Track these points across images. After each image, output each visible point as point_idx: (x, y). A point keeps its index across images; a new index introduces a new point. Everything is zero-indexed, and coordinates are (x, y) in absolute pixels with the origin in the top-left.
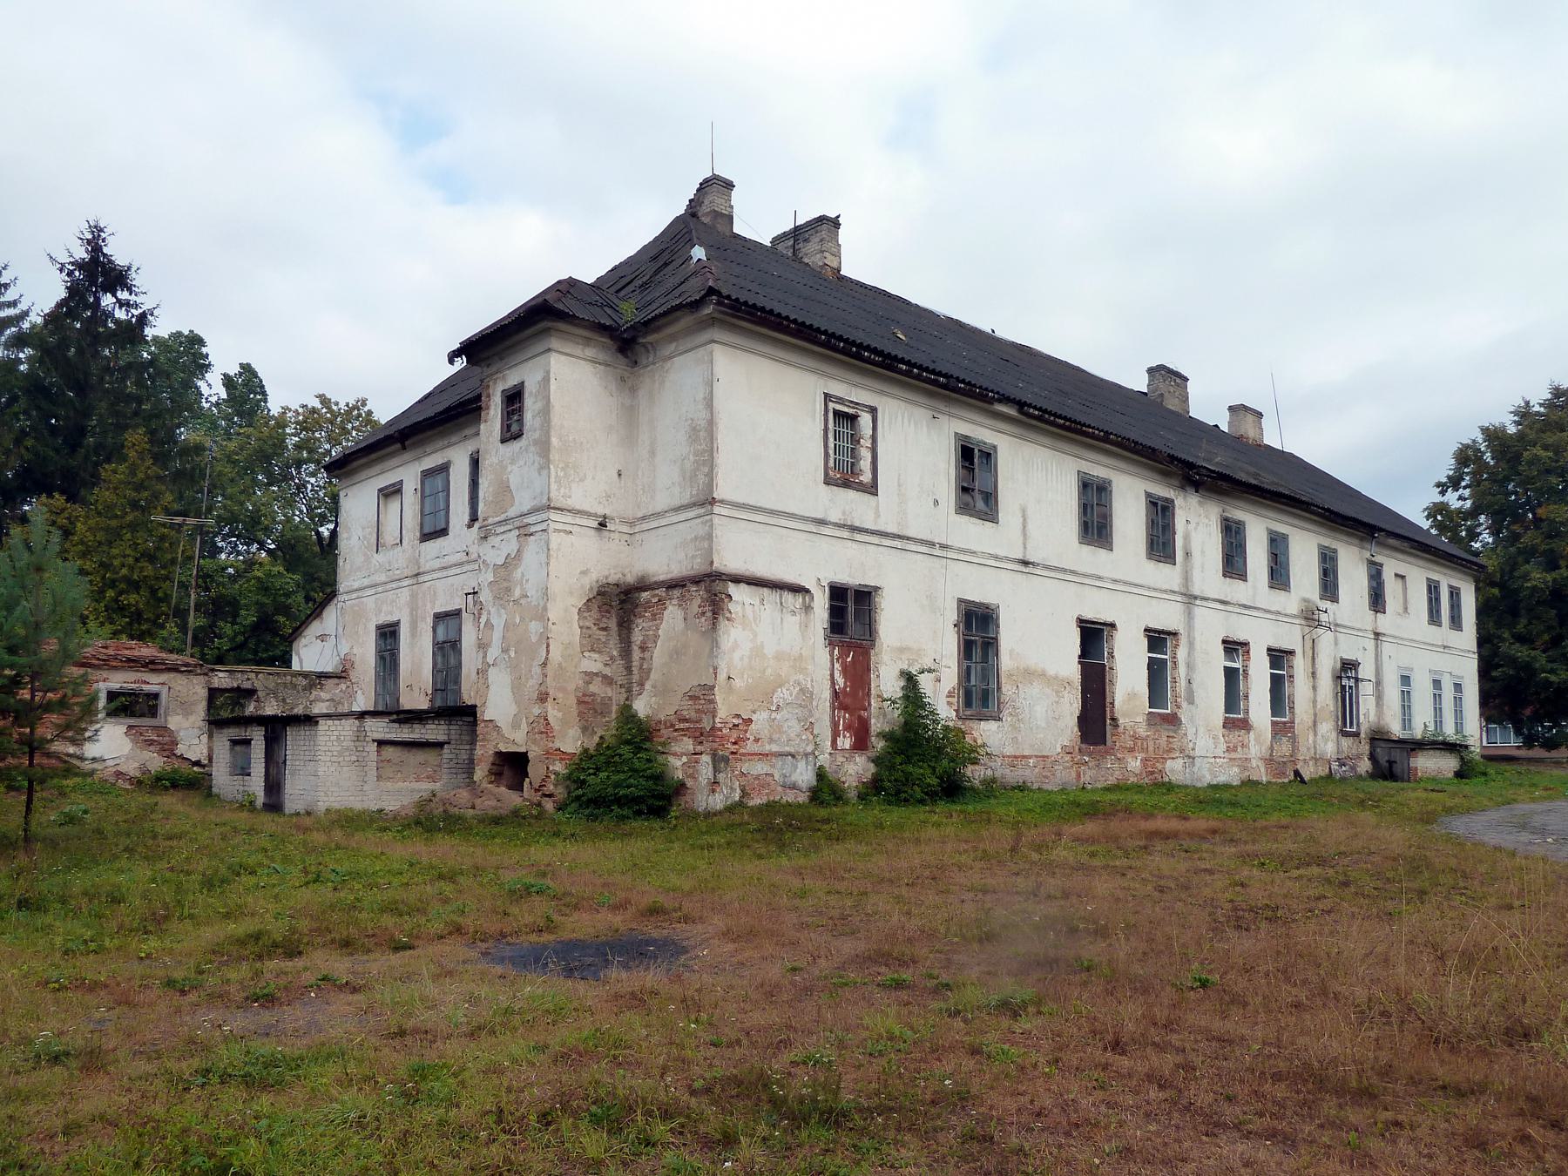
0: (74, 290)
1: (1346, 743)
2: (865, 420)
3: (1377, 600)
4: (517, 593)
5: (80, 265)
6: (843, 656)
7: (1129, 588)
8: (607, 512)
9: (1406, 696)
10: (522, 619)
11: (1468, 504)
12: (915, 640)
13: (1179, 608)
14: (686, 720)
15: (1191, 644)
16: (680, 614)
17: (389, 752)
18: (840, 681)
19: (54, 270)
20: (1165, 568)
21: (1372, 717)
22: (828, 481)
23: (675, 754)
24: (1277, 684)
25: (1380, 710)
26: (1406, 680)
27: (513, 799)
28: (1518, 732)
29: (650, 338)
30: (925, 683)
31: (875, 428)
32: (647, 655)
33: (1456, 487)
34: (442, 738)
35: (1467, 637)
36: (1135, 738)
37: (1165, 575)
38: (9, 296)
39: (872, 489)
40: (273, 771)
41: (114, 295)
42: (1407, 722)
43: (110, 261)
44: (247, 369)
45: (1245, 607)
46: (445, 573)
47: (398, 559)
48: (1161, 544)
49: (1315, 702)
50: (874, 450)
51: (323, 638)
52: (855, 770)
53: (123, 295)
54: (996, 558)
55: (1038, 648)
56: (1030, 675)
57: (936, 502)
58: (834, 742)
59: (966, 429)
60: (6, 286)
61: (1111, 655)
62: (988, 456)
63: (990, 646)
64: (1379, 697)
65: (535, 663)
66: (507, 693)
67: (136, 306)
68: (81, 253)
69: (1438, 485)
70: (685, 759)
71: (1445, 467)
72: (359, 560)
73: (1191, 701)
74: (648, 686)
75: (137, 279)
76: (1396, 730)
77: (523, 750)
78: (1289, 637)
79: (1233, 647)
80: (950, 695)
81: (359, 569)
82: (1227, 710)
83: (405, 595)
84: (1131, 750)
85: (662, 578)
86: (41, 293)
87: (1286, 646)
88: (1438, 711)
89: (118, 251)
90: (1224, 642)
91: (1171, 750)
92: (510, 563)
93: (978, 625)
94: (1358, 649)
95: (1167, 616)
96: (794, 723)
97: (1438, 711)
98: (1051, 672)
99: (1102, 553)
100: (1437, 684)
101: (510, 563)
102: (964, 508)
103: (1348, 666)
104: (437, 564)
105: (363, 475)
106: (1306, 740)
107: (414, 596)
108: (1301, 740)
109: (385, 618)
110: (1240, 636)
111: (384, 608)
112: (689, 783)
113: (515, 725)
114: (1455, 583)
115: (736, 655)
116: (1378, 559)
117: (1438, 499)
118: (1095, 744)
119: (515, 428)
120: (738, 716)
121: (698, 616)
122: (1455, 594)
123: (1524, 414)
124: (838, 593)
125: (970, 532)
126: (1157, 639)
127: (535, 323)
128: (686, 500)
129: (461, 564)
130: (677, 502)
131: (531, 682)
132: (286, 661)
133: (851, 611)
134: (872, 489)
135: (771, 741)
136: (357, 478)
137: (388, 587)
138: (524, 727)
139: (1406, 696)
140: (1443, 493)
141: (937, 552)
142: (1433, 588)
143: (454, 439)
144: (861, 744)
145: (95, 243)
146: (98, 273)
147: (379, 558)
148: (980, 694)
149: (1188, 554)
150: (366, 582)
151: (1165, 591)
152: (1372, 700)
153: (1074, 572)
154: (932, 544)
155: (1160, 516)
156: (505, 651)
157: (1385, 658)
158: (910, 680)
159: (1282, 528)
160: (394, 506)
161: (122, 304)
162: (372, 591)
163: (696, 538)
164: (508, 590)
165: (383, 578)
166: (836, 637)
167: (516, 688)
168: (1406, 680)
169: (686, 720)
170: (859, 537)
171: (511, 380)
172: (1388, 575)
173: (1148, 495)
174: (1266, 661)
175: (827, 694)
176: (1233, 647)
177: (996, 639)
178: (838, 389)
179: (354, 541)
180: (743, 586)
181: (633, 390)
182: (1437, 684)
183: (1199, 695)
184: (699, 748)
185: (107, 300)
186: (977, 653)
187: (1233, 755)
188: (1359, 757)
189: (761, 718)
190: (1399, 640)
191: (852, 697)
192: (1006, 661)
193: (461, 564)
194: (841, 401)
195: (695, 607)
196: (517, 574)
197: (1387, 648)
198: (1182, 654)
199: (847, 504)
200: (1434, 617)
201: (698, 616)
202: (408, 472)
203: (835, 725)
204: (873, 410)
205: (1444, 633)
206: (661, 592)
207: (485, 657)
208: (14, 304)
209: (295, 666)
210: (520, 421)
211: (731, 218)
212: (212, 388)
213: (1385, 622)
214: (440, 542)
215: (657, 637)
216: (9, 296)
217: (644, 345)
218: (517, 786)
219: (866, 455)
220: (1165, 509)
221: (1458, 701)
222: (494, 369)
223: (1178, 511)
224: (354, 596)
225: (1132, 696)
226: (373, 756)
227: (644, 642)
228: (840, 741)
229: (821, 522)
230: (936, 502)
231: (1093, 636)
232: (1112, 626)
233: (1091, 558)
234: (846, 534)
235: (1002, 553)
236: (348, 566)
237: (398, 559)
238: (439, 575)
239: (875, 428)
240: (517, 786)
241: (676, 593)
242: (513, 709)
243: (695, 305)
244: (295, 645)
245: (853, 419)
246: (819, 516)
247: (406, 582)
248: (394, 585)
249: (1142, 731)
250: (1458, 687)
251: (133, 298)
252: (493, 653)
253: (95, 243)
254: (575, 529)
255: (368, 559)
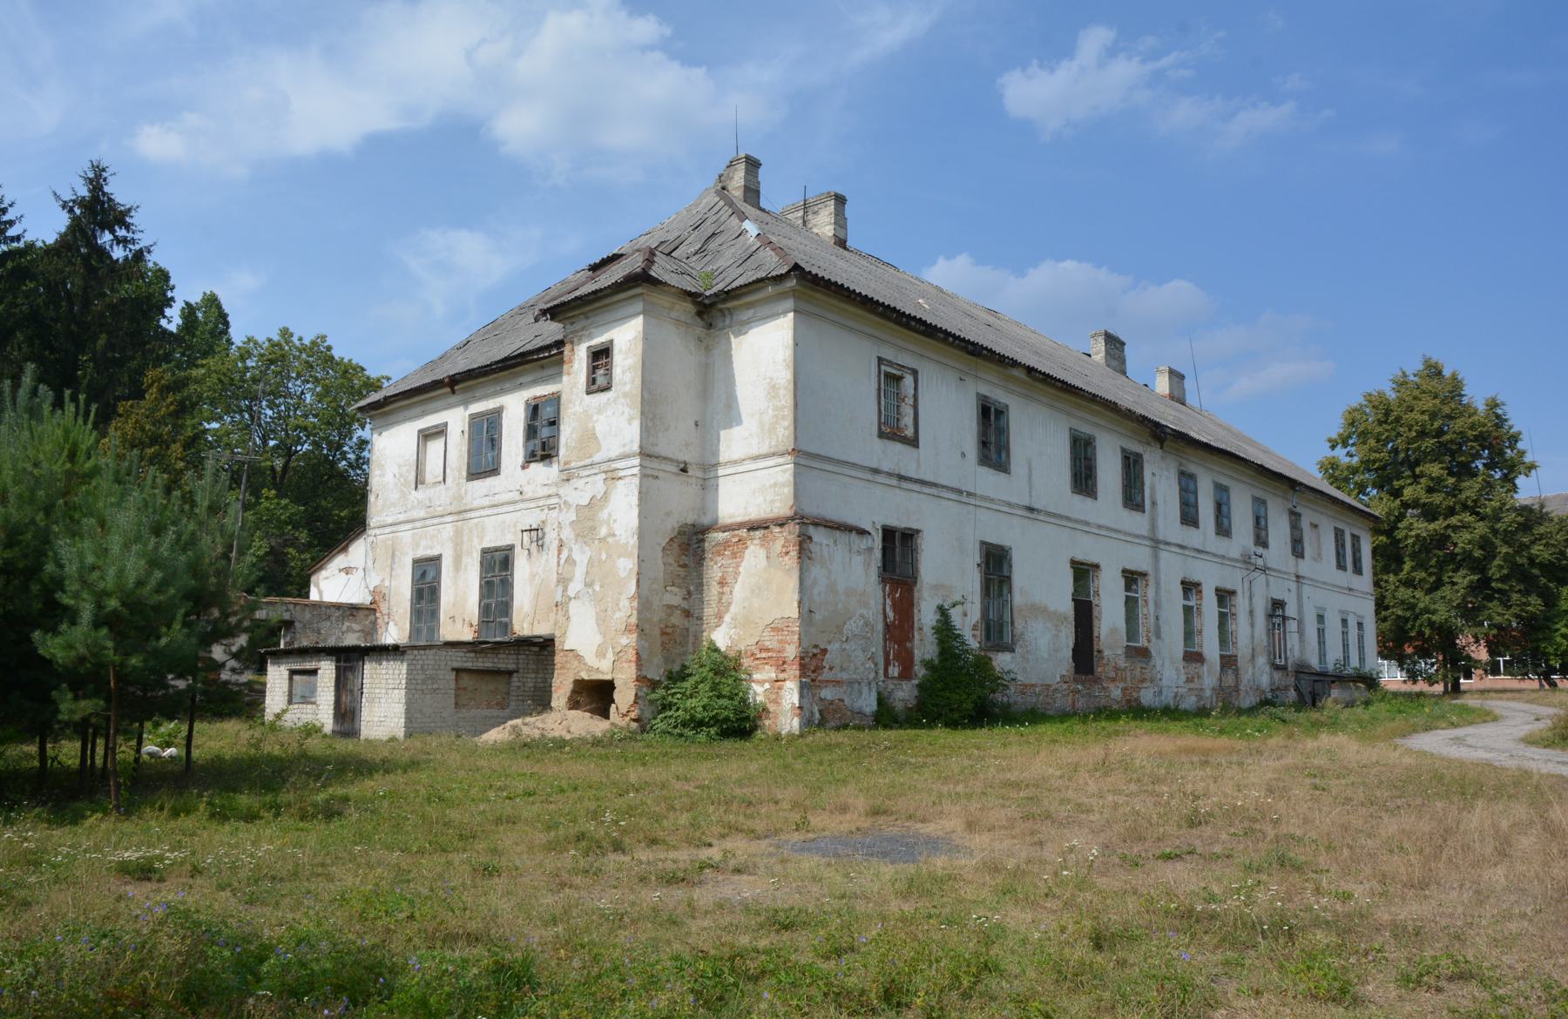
0: (76, 227)
1: (1277, 675)
2: (908, 380)
3: (1297, 549)
4: (603, 532)
5: (81, 202)
6: (893, 591)
7: (1109, 533)
8: (687, 458)
9: (1321, 632)
10: (609, 556)
11: (1356, 459)
12: (947, 577)
13: (1148, 551)
14: (768, 650)
15: (1158, 584)
16: (762, 553)
17: (466, 680)
18: (891, 614)
19: (57, 206)
20: (1137, 516)
21: (1297, 654)
22: (881, 435)
23: (758, 682)
24: (1223, 619)
25: (1302, 648)
26: (1321, 618)
27: (599, 726)
28: (1401, 666)
29: (729, 305)
30: (956, 616)
31: (916, 389)
32: (726, 589)
33: (1345, 445)
34: (512, 667)
35: (1365, 582)
36: (1117, 669)
37: (1136, 522)
38: (11, 232)
39: (914, 442)
40: (345, 699)
41: (113, 232)
42: (1322, 656)
43: (110, 200)
44: (212, 301)
45: (1198, 551)
46: (495, 511)
47: (441, 497)
48: (1133, 497)
49: (1253, 637)
50: (915, 407)
51: (347, 570)
52: (904, 694)
53: (121, 233)
54: (1009, 504)
55: (1042, 587)
56: (1038, 610)
57: (963, 455)
58: (886, 670)
59: (985, 390)
60: (11, 223)
61: (1097, 593)
62: (1001, 413)
63: (1006, 581)
64: (1301, 631)
65: (623, 597)
66: (591, 623)
67: (133, 241)
68: (84, 192)
69: (1330, 440)
70: (767, 686)
71: (1336, 428)
72: (394, 496)
73: (1158, 636)
74: (727, 618)
75: (135, 219)
76: (1314, 662)
77: (608, 677)
78: (1232, 578)
79: (1190, 587)
80: (975, 628)
81: (393, 505)
82: (1186, 645)
83: (448, 531)
84: (1113, 680)
85: (739, 519)
86: (43, 225)
87: (1229, 586)
88: (1345, 646)
89: (119, 191)
90: (1183, 583)
91: (1143, 681)
92: (595, 505)
93: (995, 563)
94: (1282, 589)
95: (1139, 559)
96: (859, 653)
97: (1345, 646)
98: (1052, 608)
99: (1089, 501)
100: (1344, 622)
101: (595, 505)
102: (985, 460)
103: (1278, 605)
104: (486, 501)
105: (401, 415)
106: (1246, 676)
107: (458, 533)
108: (1242, 672)
109: (423, 552)
110: (1195, 578)
111: (423, 543)
112: (771, 707)
113: (601, 654)
114: (1356, 532)
115: (816, 591)
116: (1298, 510)
117: (1330, 453)
118: (1086, 674)
119: (601, 381)
120: (816, 646)
121: (781, 555)
122: (1355, 538)
123: (1401, 383)
124: (889, 534)
125: (987, 481)
126: (1132, 578)
127: (630, 288)
128: (764, 449)
129: (515, 502)
130: (755, 451)
131: (617, 615)
132: (303, 588)
133: (898, 547)
134: (914, 442)
135: (842, 669)
136: (392, 418)
137: (429, 522)
138: (610, 656)
139: (1321, 632)
140: (1333, 447)
141: (964, 499)
142: (1339, 534)
143: (507, 385)
144: (906, 674)
145: (96, 181)
146: (97, 211)
147: (421, 495)
148: (997, 632)
149: (1154, 503)
150: (402, 517)
151: (1125, 534)
152: (1296, 636)
153: (1068, 519)
154: (959, 492)
155: (1132, 466)
156: (588, 585)
157: (1305, 600)
158: (943, 611)
159: (1224, 481)
160: (435, 447)
161: (124, 242)
162: (409, 526)
163: (775, 484)
164: (593, 529)
165: (422, 514)
166: (887, 575)
167: (602, 620)
168: (1321, 618)
169: (768, 650)
170: (905, 485)
171: (599, 340)
172: (1305, 524)
173: (1123, 450)
174: (1215, 599)
175: (880, 627)
176: (1190, 587)
177: (1009, 578)
178: (888, 354)
179: (389, 478)
180: (822, 529)
181: (708, 349)
182: (1344, 622)
183: (1164, 629)
184: (781, 676)
185: (106, 238)
186: (994, 589)
187: (1191, 685)
188: (1286, 688)
189: (834, 647)
190: (1315, 583)
191: (899, 629)
192: (1018, 599)
193: (515, 502)
194: (890, 364)
195: (778, 546)
196: (604, 515)
197: (1307, 590)
198: (1151, 592)
199: (893, 456)
200: (1341, 566)
201: (781, 555)
202: (456, 418)
203: (887, 654)
204: (915, 373)
205: (1347, 578)
206: (743, 532)
207: (565, 590)
208: (18, 238)
209: (314, 596)
210: (609, 373)
211: (758, 192)
212: (172, 320)
213: (1305, 567)
214: (490, 482)
215: (737, 574)
216: (11, 232)
217: (721, 311)
218: (605, 714)
219: (907, 411)
220: (1136, 462)
221: (1361, 638)
222: (577, 326)
223: (1146, 466)
224: (388, 530)
225: (1113, 631)
226: (453, 685)
227: (723, 578)
228: (891, 669)
229: (876, 471)
230: (963, 455)
231: (1083, 572)
232: (1097, 567)
233: (1080, 506)
234: (894, 482)
235: (1014, 500)
236: (380, 502)
237: (441, 497)
238: (489, 512)
239: (916, 389)
240: (605, 714)
241: (758, 533)
242: (598, 639)
243: (779, 279)
244: (313, 579)
245: (899, 379)
246: (874, 466)
247: (450, 519)
248: (435, 521)
249: (1122, 663)
250: (1360, 625)
251: (130, 235)
252: (575, 587)
253: (96, 181)
254: (661, 474)
255: (404, 496)
